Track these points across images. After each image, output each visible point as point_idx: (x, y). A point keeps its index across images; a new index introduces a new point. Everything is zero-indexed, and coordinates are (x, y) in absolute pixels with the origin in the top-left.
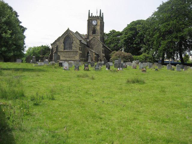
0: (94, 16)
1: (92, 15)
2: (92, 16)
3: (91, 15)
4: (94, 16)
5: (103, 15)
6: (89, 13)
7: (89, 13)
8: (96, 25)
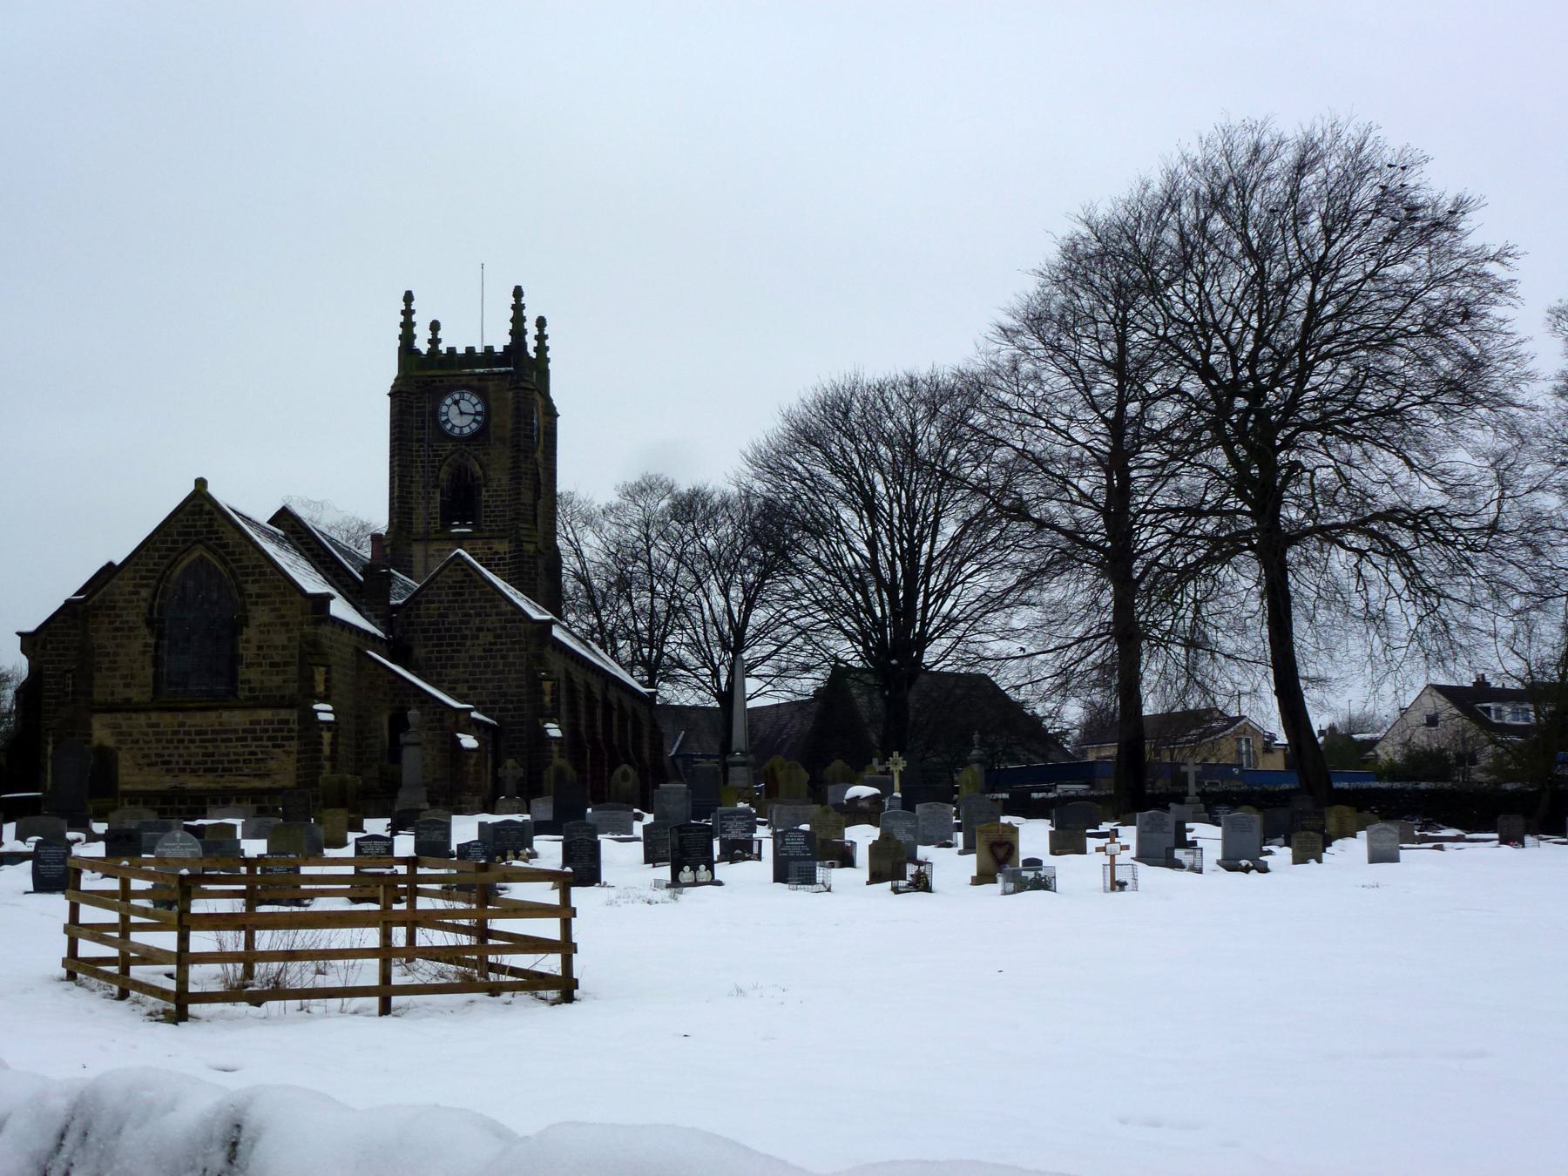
0: (451, 350)
1: (434, 341)
3: (422, 345)
4: (461, 350)
5: (541, 338)
6: (408, 326)
7: (408, 326)
8: (474, 436)
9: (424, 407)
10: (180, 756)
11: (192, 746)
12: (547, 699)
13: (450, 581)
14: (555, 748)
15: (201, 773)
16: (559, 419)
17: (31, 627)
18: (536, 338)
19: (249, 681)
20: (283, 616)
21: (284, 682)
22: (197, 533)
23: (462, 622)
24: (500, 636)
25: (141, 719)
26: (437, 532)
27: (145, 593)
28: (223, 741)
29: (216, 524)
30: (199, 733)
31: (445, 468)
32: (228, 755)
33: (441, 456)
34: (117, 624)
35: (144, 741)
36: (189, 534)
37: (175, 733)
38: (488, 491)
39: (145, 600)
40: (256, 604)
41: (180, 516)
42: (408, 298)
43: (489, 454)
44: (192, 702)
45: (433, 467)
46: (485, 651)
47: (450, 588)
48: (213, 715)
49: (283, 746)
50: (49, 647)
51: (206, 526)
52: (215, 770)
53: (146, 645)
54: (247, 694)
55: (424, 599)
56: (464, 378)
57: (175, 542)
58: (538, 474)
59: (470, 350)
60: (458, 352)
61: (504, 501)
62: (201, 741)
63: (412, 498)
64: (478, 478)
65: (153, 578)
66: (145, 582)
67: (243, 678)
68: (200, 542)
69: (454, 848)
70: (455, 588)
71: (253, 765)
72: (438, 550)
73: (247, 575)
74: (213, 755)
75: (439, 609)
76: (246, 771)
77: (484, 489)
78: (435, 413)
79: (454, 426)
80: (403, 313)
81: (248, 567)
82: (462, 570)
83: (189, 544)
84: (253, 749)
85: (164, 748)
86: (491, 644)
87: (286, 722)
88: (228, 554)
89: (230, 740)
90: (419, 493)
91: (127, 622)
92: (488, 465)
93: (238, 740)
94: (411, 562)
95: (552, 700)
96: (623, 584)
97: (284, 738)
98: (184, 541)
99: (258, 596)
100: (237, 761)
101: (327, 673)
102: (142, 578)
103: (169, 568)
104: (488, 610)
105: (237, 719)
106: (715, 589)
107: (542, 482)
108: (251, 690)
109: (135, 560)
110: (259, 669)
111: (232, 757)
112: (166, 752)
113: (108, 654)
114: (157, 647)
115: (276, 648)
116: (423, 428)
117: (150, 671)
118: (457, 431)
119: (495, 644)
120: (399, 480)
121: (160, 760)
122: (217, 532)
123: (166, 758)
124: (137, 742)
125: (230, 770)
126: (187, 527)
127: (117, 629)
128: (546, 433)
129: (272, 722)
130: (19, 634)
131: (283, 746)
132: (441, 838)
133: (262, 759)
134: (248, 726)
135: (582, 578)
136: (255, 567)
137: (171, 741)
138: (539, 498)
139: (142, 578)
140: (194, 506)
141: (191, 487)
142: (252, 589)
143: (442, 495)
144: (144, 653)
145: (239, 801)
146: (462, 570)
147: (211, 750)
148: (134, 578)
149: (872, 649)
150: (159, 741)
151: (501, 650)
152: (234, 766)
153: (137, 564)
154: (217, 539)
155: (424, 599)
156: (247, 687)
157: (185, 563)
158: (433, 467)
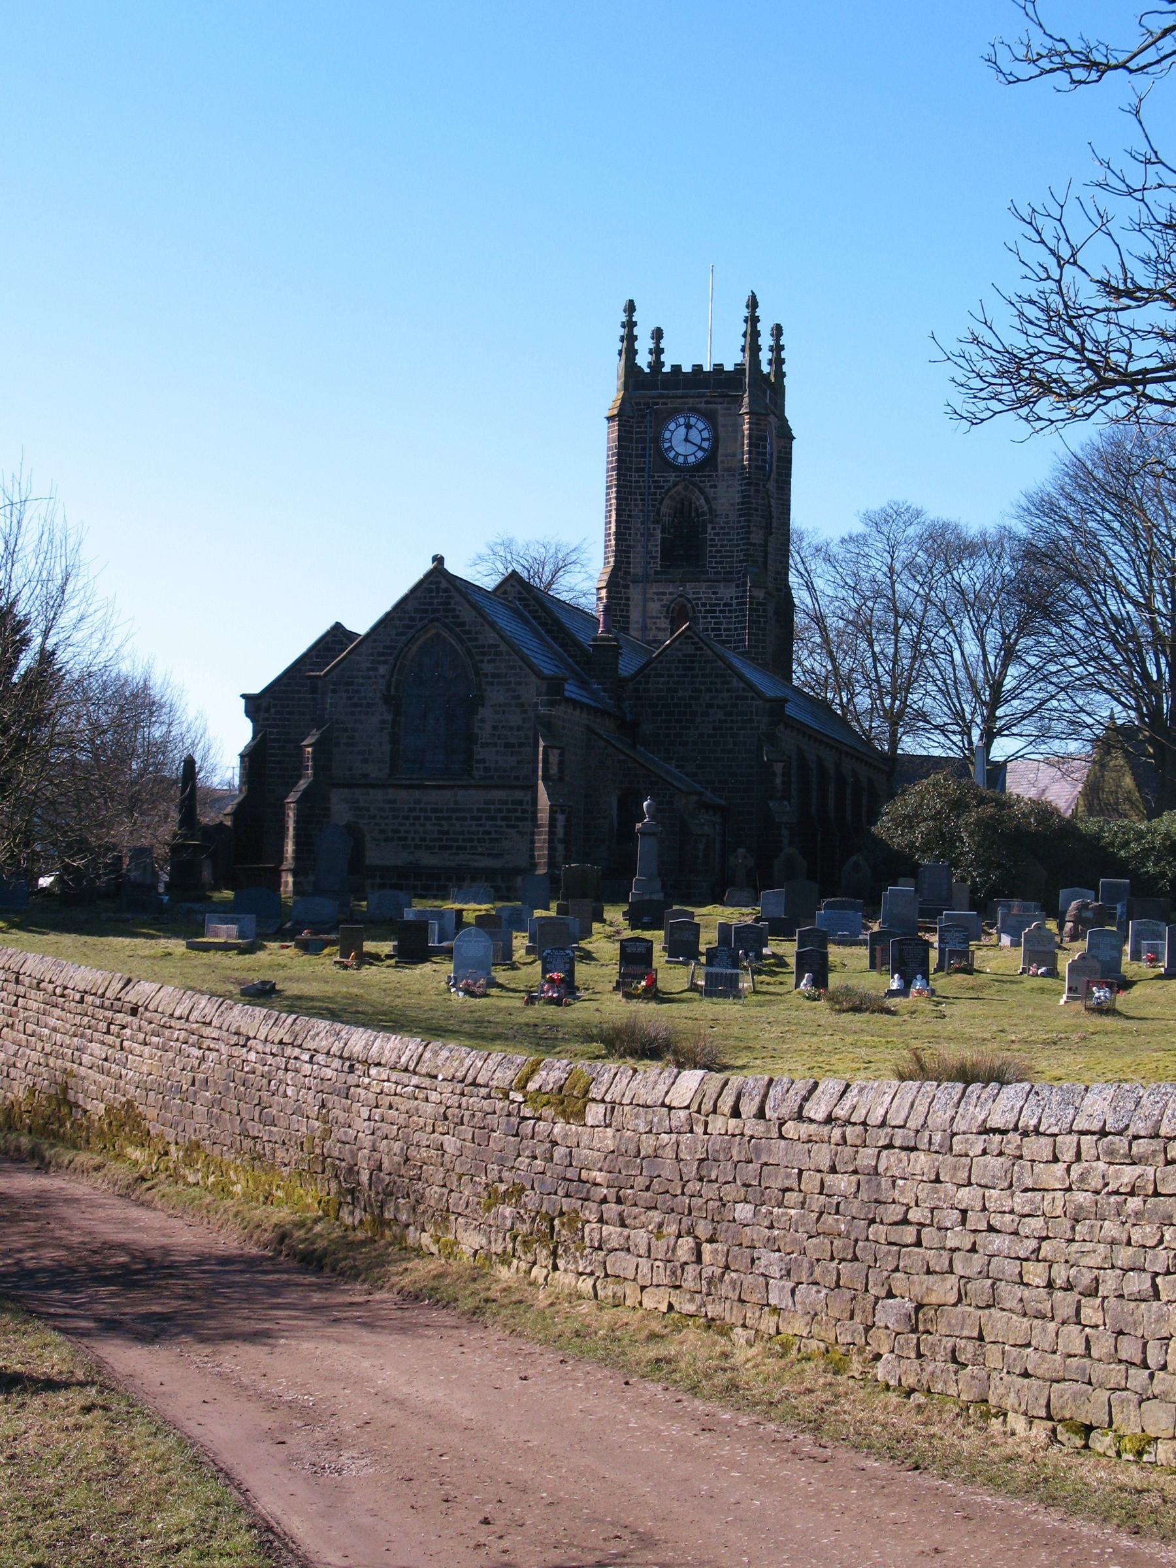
0: (677, 368)
1: (657, 351)
2: (657, 365)
3: (643, 360)
4: (687, 368)
5: (777, 348)
6: (630, 339)
7: (630, 339)
8: (700, 466)
9: (645, 432)
10: (416, 832)
11: (428, 823)
12: (778, 781)
13: (680, 654)
14: (785, 832)
15: (436, 850)
16: (794, 443)
17: (256, 689)
18: (771, 349)
19: (484, 761)
20: (518, 697)
21: (519, 762)
22: (434, 611)
23: (691, 698)
24: (730, 714)
25: (379, 794)
26: (656, 573)
27: (382, 670)
28: (458, 819)
29: (452, 601)
30: (434, 811)
31: (667, 502)
32: (462, 833)
33: (663, 487)
34: (355, 700)
35: (382, 817)
36: (426, 611)
37: (411, 810)
38: (713, 528)
39: (383, 676)
40: (492, 684)
41: (418, 594)
42: (631, 308)
43: (715, 486)
44: (429, 780)
45: (653, 500)
46: (714, 728)
47: (679, 661)
48: (448, 794)
49: (517, 826)
50: (273, 710)
51: (441, 604)
52: (450, 848)
53: (383, 722)
54: (482, 773)
55: (653, 673)
56: (691, 400)
57: (412, 619)
58: (770, 506)
59: (698, 368)
60: (684, 370)
61: (732, 540)
62: (438, 818)
63: (630, 535)
64: (704, 514)
65: (391, 655)
66: (382, 658)
67: (480, 757)
68: (437, 620)
69: (703, 948)
70: (685, 662)
71: (487, 845)
72: (658, 594)
73: (483, 654)
74: (447, 833)
75: (668, 683)
76: (480, 850)
77: (709, 526)
78: (657, 439)
79: (677, 454)
80: (623, 325)
81: (483, 646)
82: (693, 643)
83: (426, 621)
84: (487, 828)
85: (400, 824)
86: (721, 721)
87: (521, 802)
88: (465, 632)
89: (465, 819)
90: (638, 529)
91: (365, 698)
92: (715, 499)
93: (473, 818)
94: (628, 605)
95: (783, 783)
96: (863, 627)
97: (517, 819)
98: (422, 619)
99: (494, 676)
100: (472, 840)
101: (561, 755)
102: (380, 654)
103: (406, 645)
104: (719, 686)
105: (474, 798)
106: (968, 632)
107: (774, 514)
108: (486, 769)
109: (373, 637)
110: (494, 749)
111: (467, 836)
112: (403, 828)
113: (346, 730)
114: (395, 723)
115: (511, 728)
116: (644, 456)
117: (387, 747)
118: (681, 460)
119: (725, 721)
120: (617, 515)
121: (396, 835)
122: (454, 610)
123: (403, 834)
124: (374, 817)
125: (465, 848)
126: (424, 604)
127: (355, 705)
128: (779, 459)
129: (506, 803)
130: (243, 696)
131: (517, 826)
132: (692, 938)
133: (497, 839)
134: (483, 806)
135: (819, 620)
136: (491, 646)
137: (407, 818)
138: (771, 534)
139: (380, 654)
140: (431, 583)
141: (429, 566)
142: (488, 668)
143: (663, 532)
144: (382, 730)
145: (473, 879)
146: (693, 643)
147: (446, 828)
148: (372, 655)
149: (1146, 715)
150: (395, 817)
151: (731, 728)
152: (468, 845)
153: (375, 641)
154: (453, 617)
155: (653, 673)
156: (481, 766)
157: (422, 639)
158: (653, 500)
